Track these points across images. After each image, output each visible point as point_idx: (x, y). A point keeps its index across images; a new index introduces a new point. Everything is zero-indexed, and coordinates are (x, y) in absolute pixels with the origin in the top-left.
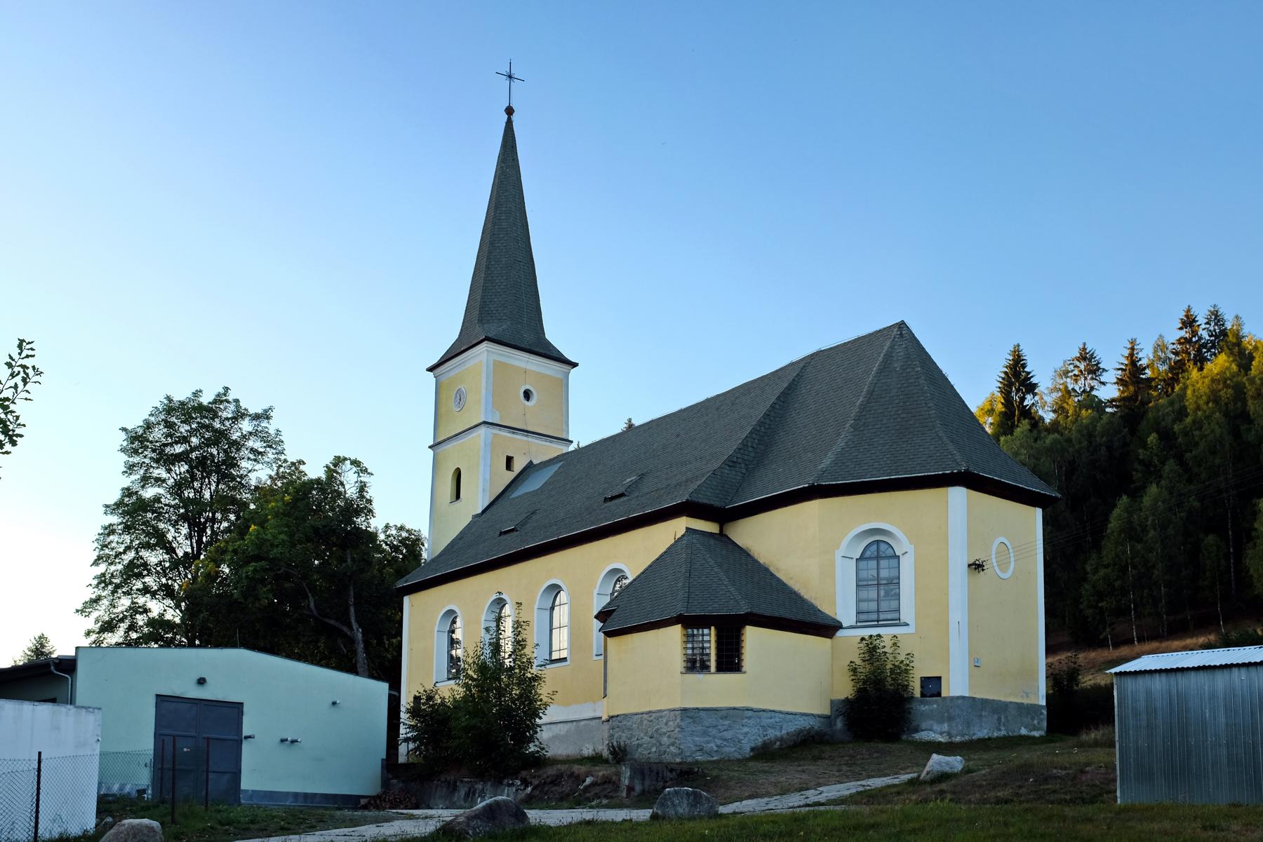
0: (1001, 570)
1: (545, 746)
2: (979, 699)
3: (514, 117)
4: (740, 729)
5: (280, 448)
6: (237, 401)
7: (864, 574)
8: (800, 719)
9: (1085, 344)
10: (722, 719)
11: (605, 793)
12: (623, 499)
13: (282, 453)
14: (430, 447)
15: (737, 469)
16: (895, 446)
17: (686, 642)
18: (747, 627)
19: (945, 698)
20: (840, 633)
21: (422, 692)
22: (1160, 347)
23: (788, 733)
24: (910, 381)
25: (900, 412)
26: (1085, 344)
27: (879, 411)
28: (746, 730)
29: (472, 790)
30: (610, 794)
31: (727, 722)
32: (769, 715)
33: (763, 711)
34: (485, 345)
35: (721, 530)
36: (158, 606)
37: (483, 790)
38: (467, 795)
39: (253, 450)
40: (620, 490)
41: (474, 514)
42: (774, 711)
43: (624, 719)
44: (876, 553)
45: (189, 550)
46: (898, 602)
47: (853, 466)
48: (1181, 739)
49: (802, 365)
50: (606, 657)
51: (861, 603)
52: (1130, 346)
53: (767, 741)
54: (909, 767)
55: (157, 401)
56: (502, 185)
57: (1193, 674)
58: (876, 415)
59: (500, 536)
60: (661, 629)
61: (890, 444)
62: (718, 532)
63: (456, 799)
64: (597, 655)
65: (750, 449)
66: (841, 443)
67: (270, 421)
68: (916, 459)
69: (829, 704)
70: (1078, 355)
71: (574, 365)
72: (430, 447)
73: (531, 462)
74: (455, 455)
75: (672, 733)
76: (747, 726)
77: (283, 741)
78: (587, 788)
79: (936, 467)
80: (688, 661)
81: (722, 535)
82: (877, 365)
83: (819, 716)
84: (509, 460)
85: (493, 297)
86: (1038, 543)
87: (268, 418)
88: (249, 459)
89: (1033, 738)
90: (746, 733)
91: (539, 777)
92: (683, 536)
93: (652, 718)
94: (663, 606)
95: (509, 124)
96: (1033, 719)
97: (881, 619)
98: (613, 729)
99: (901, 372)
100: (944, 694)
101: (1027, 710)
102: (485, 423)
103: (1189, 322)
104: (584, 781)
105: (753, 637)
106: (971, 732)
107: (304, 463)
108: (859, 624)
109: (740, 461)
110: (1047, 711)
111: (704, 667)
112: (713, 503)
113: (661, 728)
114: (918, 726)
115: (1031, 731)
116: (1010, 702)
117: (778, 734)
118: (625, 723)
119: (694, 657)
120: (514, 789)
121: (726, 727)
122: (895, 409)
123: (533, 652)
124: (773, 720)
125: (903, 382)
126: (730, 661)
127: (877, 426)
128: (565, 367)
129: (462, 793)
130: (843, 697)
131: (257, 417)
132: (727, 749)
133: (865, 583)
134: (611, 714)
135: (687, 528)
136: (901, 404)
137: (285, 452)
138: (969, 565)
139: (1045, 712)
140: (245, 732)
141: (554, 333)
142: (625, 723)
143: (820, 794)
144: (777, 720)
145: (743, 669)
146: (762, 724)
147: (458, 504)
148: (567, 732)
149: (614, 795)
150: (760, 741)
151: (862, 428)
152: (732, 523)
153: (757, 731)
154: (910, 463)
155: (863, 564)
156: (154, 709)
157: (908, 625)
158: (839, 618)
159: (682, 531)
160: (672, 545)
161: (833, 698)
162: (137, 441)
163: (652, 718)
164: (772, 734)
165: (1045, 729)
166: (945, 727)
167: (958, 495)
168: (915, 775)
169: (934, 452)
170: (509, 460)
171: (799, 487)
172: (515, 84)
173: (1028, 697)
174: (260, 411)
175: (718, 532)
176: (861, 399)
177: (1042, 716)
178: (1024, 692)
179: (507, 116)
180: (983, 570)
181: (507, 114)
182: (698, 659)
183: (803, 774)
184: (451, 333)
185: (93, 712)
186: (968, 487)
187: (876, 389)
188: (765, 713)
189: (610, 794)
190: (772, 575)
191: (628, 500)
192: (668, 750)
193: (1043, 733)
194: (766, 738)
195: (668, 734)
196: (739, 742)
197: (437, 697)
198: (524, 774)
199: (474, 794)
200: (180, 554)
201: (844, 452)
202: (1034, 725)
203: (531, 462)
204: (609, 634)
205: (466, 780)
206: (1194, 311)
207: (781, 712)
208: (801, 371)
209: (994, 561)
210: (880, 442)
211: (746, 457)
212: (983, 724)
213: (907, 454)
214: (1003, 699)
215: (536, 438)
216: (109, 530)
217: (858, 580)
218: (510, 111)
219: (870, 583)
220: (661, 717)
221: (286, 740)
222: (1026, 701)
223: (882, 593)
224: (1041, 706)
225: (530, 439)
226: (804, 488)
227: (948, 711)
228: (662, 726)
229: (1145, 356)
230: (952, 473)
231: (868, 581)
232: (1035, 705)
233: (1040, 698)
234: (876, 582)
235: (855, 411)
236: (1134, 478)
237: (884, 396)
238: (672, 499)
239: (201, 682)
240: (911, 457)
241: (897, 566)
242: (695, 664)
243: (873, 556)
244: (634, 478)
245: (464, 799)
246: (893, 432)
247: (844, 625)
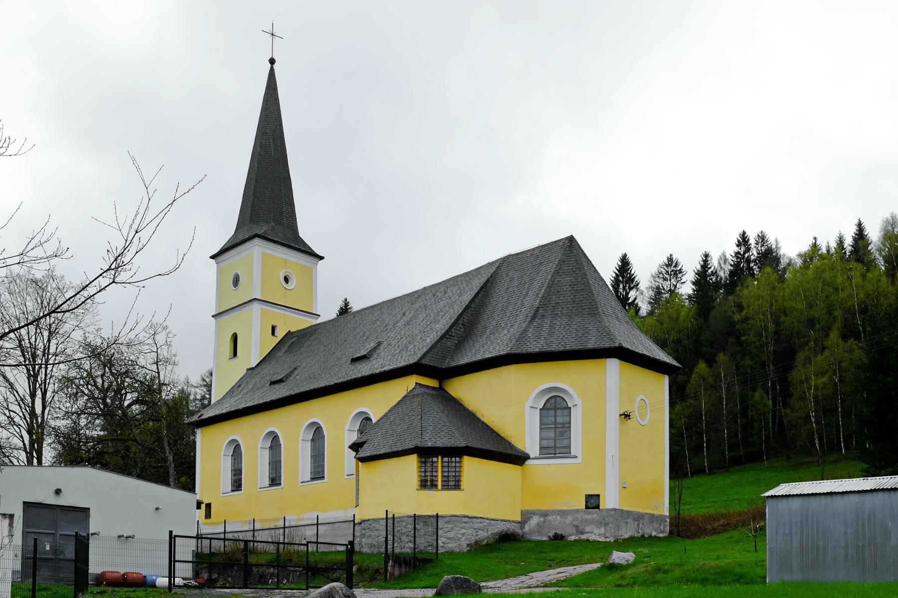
0: (641, 419)
3: (275, 66)
4: (459, 531)
7: (545, 420)
8: (500, 524)
10: (446, 523)
14: (213, 316)
15: (452, 340)
17: (460, 472)
18: (465, 456)
20: (528, 462)
28: (464, 531)
31: (450, 526)
32: (480, 520)
33: (476, 518)
34: (257, 241)
40: (363, 353)
41: (248, 368)
42: (482, 518)
44: (559, 407)
46: (569, 440)
48: (770, 538)
49: (497, 264)
50: (358, 476)
51: (542, 441)
53: (478, 539)
57: (823, 497)
60: (401, 457)
62: (438, 386)
64: (302, 483)
69: (520, 512)
71: (322, 258)
72: (213, 316)
73: (289, 331)
74: (232, 323)
76: (464, 528)
77: (119, 537)
80: (422, 481)
81: (441, 389)
84: (273, 328)
89: (659, 538)
90: (464, 534)
95: (272, 74)
96: (660, 525)
97: (557, 453)
98: (365, 529)
100: (601, 507)
101: (655, 519)
102: (255, 299)
103: (744, 241)
105: (469, 464)
106: (620, 534)
108: (541, 456)
111: (433, 486)
112: (435, 365)
114: (584, 529)
115: (659, 533)
116: (646, 514)
117: (486, 535)
119: (426, 478)
121: (449, 529)
124: (482, 524)
126: (454, 483)
132: (450, 545)
133: (546, 426)
135: (416, 383)
138: (620, 415)
139: (668, 520)
140: (91, 531)
143: (531, 579)
144: (485, 524)
145: (462, 488)
146: (474, 527)
147: (235, 360)
150: (473, 539)
152: (447, 380)
153: (471, 532)
155: (545, 412)
156: (22, 513)
157: (577, 457)
158: (528, 451)
159: (413, 385)
161: (523, 509)
164: (482, 535)
166: (602, 530)
167: (613, 365)
170: (273, 328)
172: (276, 40)
173: (657, 509)
175: (438, 386)
178: (655, 506)
179: (270, 65)
180: (629, 419)
181: (270, 63)
182: (429, 479)
184: (227, 230)
186: (619, 359)
188: (476, 519)
190: (478, 419)
192: (407, 545)
193: (666, 534)
196: (458, 540)
202: (661, 529)
203: (289, 331)
204: (363, 460)
207: (487, 519)
208: (496, 270)
209: (637, 413)
212: (628, 529)
215: (280, 309)
217: (541, 424)
218: (272, 61)
219: (550, 426)
221: (123, 536)
223: (558, 433)
224: (665, 516)
225: (287, 313)
227: (604, 519)
229: (714, 262)
231: (548, 424)
234: (553, 426)
239: (58, 492)
241: (569, 414)
242: (426, 483)
243: (551, 407)
247: (531, 457)
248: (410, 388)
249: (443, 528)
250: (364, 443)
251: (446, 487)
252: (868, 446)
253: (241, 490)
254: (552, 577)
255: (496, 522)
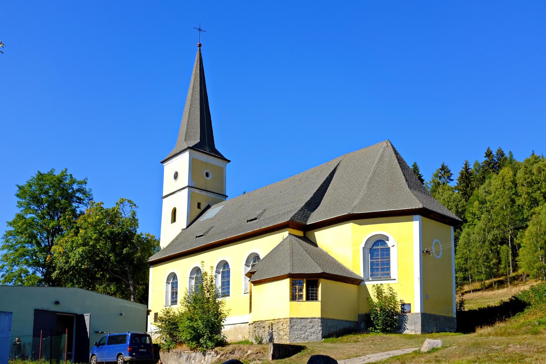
1: (226, 336)
2: (428, 314)
5: (91, 197)
6: (71, 175)
8: (345, 323)
9: (444, 163)
11: (258, 358)
12: (256, 221)
13: (92, 199)
16: (387, 196)
19: (412, 314)
21: (164, 309)
22: (476, 164)
23: (339, 330)
24: (393, 167)
25: (389, 181)
26: (444, 163)
27: (379, 180)
29: (189, 356)
30: (261, 359)
33: (328, 319)
35: (304, 234)
36: (32, 270)
37: (195, 356)
38: (187, 359)
39: (78, 198)
43: (261, 323)
45: (47, 244)
47: (368, 205)
52: (465, 163)
54: (404, 345)
55: (34, 174)
56: (196, 79)
58: (378, 182)
59: (196, 238)
61: (385, 195)
63: (181, 361)
65: (317, 198)
66: (361, 194)
67: (86, 184)
68: (398, 202)
70: (441, 167)
71: (229, 161)
75: (285, 329)
78: (248, 356)
79: (408, 205)
82: (377, 160)
83: (353, 322)
85: (192, 129)
86: (452, 242)
87: (86, 183)
88: (76, 202)
91: (223, 350)
92: (287, 237)
93: (275, 322)
94: (280, 269)
98: (255, 327)
99: (388, 162)
100: (412, 312)
103: (489, 154)
104: (247, 352)
107: (103, 204)
109: (313, 203)
110: (457, 320)
113: (280, 327)
116: (441, 316)
118: (261, 324)
120: (211, 356)
122: (387, 179)
123: (474, 234)
125: (390, 167)
127: (378, 187)
128: (225, 162)
129: (185, 358)
130: (364, 313)
131: (80, 183)
134: (254, 321)
136: (390, 177)
137: (93, 199)
139: (456, 321)
141: (217, 147)
142: (261, 324)
148: (230, 330)
149: (263, 359)
151: (371, 188)
154: (395, 204)
160: (282, 242)
162: (22, 192)
163: (275, 322)
165: (456, 329)
168: (417, 349)
169: (406, 199)
171: (343, 215)
173: (448, 313)
174: (82, 180)
176: (370, 175)
177: (454, 323)
183: (354, 349)
185: (8, 315)
187: (377, 170)
189: (261, 359)
191: (259, 221)
192: (283, 338)
194: (330, 332)
195: (283, 330)
197: (171, 312)
198: (216, 349)
199: (190, 359)
200: (43, 245)
201: (363, 199)
202: (451, 326)
204: (256, 283)
205: (186, 351)
206: (491, 149)
210: (380, 194)
211: (315, 201)
213: (393, 200)
214: (438, 314)
216: (10, 233)
220: (280, 322)
221: (98, 332)
222: (448, 315)
224: (454, 318)
226: (346, 215)
228: (280, 326)
230: (416, 209)
232: (451, 317)
233: (454, 314)
235: (367, 180)
236: (468, 221)
237: (381, 173)
238: (282, 220)
240: (396, 201)
244: (261, 211)
245: (185, 361)
246: (386, 190)
248: (285, 237)
249: (307, 326)
250: (254, 272)
251: (308, 299)
252: (309, 351)
253: (177, 304)
254: (383, 358)
255: (342, 322)
